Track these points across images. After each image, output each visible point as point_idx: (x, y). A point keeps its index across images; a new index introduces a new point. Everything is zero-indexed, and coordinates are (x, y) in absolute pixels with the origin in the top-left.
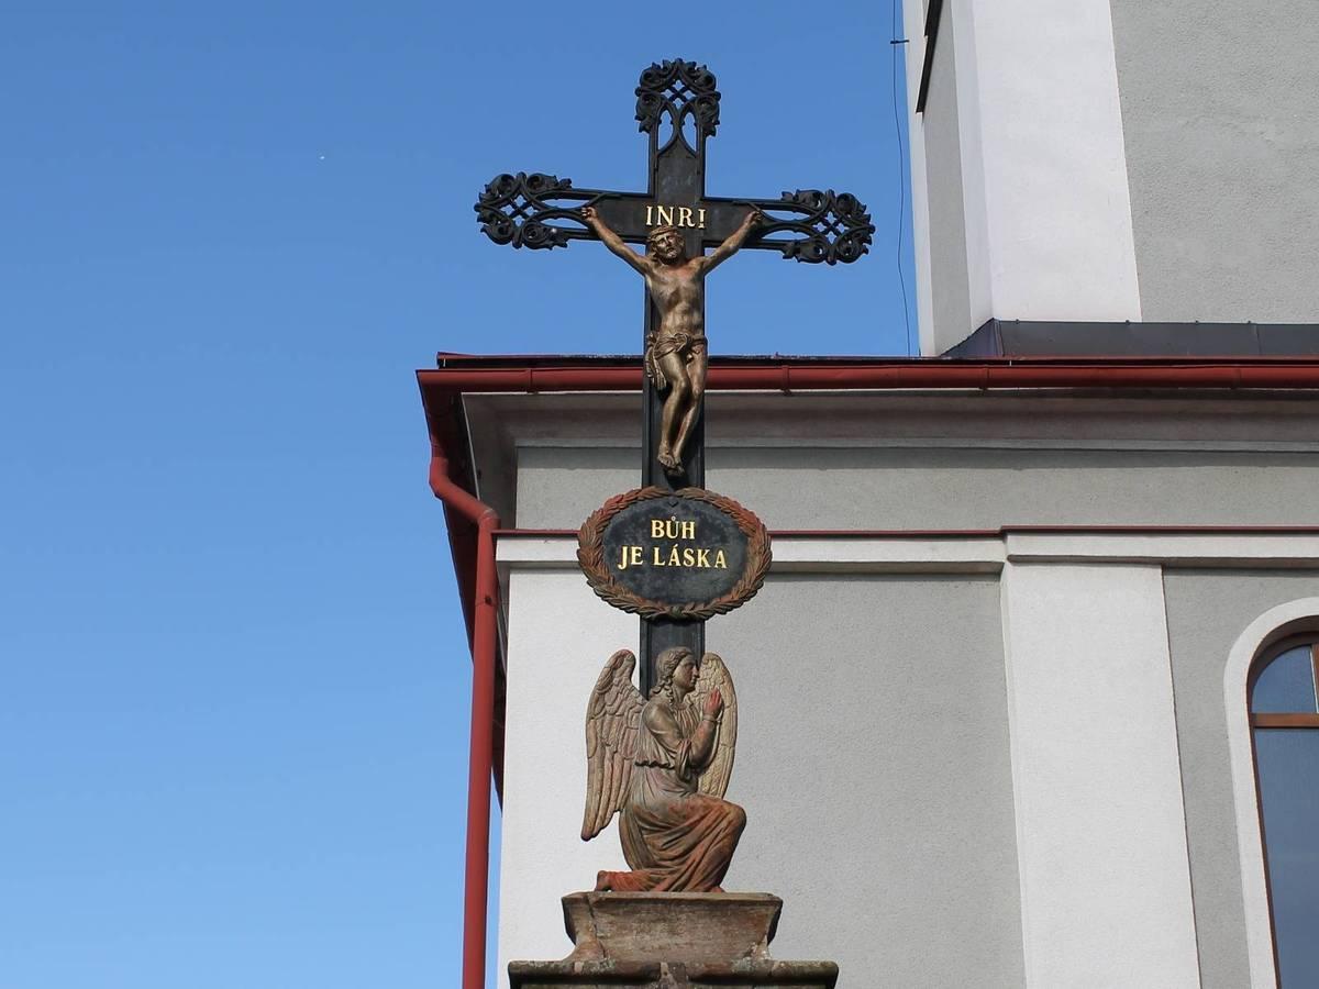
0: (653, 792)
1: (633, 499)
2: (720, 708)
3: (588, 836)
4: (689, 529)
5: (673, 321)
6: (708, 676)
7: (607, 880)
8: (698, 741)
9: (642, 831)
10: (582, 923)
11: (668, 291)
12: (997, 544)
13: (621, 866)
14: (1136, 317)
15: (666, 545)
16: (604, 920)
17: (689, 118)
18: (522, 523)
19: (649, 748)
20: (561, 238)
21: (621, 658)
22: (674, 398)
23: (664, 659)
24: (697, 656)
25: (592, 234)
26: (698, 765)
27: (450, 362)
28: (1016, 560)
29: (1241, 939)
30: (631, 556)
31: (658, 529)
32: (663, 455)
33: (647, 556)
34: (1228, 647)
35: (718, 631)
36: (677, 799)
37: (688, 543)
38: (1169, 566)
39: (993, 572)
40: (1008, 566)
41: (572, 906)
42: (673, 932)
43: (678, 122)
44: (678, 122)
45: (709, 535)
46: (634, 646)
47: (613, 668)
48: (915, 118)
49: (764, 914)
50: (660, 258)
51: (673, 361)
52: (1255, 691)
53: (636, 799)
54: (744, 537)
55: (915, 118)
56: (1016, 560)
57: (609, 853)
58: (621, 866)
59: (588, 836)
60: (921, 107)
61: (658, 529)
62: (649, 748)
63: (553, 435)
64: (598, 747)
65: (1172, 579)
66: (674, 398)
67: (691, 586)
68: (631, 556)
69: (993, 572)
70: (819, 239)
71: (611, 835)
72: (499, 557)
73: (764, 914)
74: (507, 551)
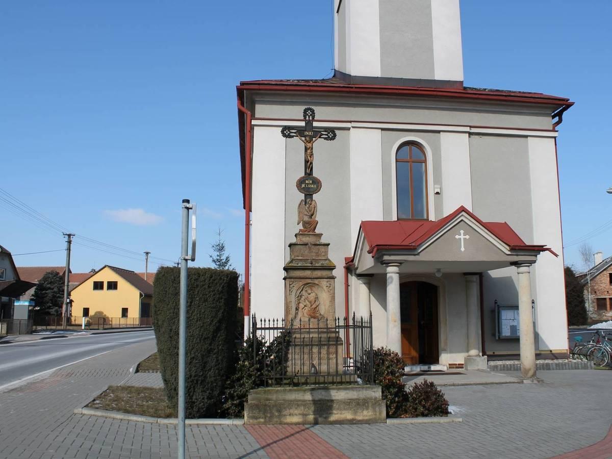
0: (306, 219)
1: (303, 177)
2: (315, 207)
3: (298, 224)
4: (311, 182)
5: (309, 151)
6: (313, 202)
7: (300, 230)
8: (312, 212)
9: (305, 224)
10: (298, 237)
11: (308, 147)
12: (350, 123)
13: (302, 228)
14: (379, 76)
15: (308, 184)
16: (301, 236)
17: (311, 117)
18: (256, 116)
19: (306, 213)
20: (293, 137)
21: (302, 200)
22: (309, 163)
23: (308, 200)
24: (312, 200)
25: (297, 136)
26: (312, 215)
27: (242, 84)
28: (353, 127)
29: (391, 202)
30: (303, 186)
31: (307, 182)
32: (307, 171)
33: (305, 186)
34: (396, 141)
35: (315, 196)
36: (310, 220)
37: (310, 184)
38: (382, 129)
39: (349, 129)
40: (351, 128)
41: (296, 236)
42: (310, 238)
43: (309, 117)
44: (309, 117)
45: (314, 183)
46: (303, 198)
47: (301, 201)
48: (336, 14)
49: (320, 235)
50: (307, 141)
51: (309, 157)
52: (398, 153)
53: (304, 220)
54: (318, 183)
55: (336, 14)
56: (353, 127)
57: (301, 227)
58: (302, 228)
59: (298, 224)
60: (338, 12)
61: (307, 182)
62: (306, 213)
63: (262, 98)
64: (300, 212)
65: (383, 132)
66: (309, 163)
67: (312, 190)
68: (303, 186)
69: (349, 129)
70: (329, 137)
71: (301, 224)
72: (252, 123)
73: (320, 235)
74: (254, 122)
